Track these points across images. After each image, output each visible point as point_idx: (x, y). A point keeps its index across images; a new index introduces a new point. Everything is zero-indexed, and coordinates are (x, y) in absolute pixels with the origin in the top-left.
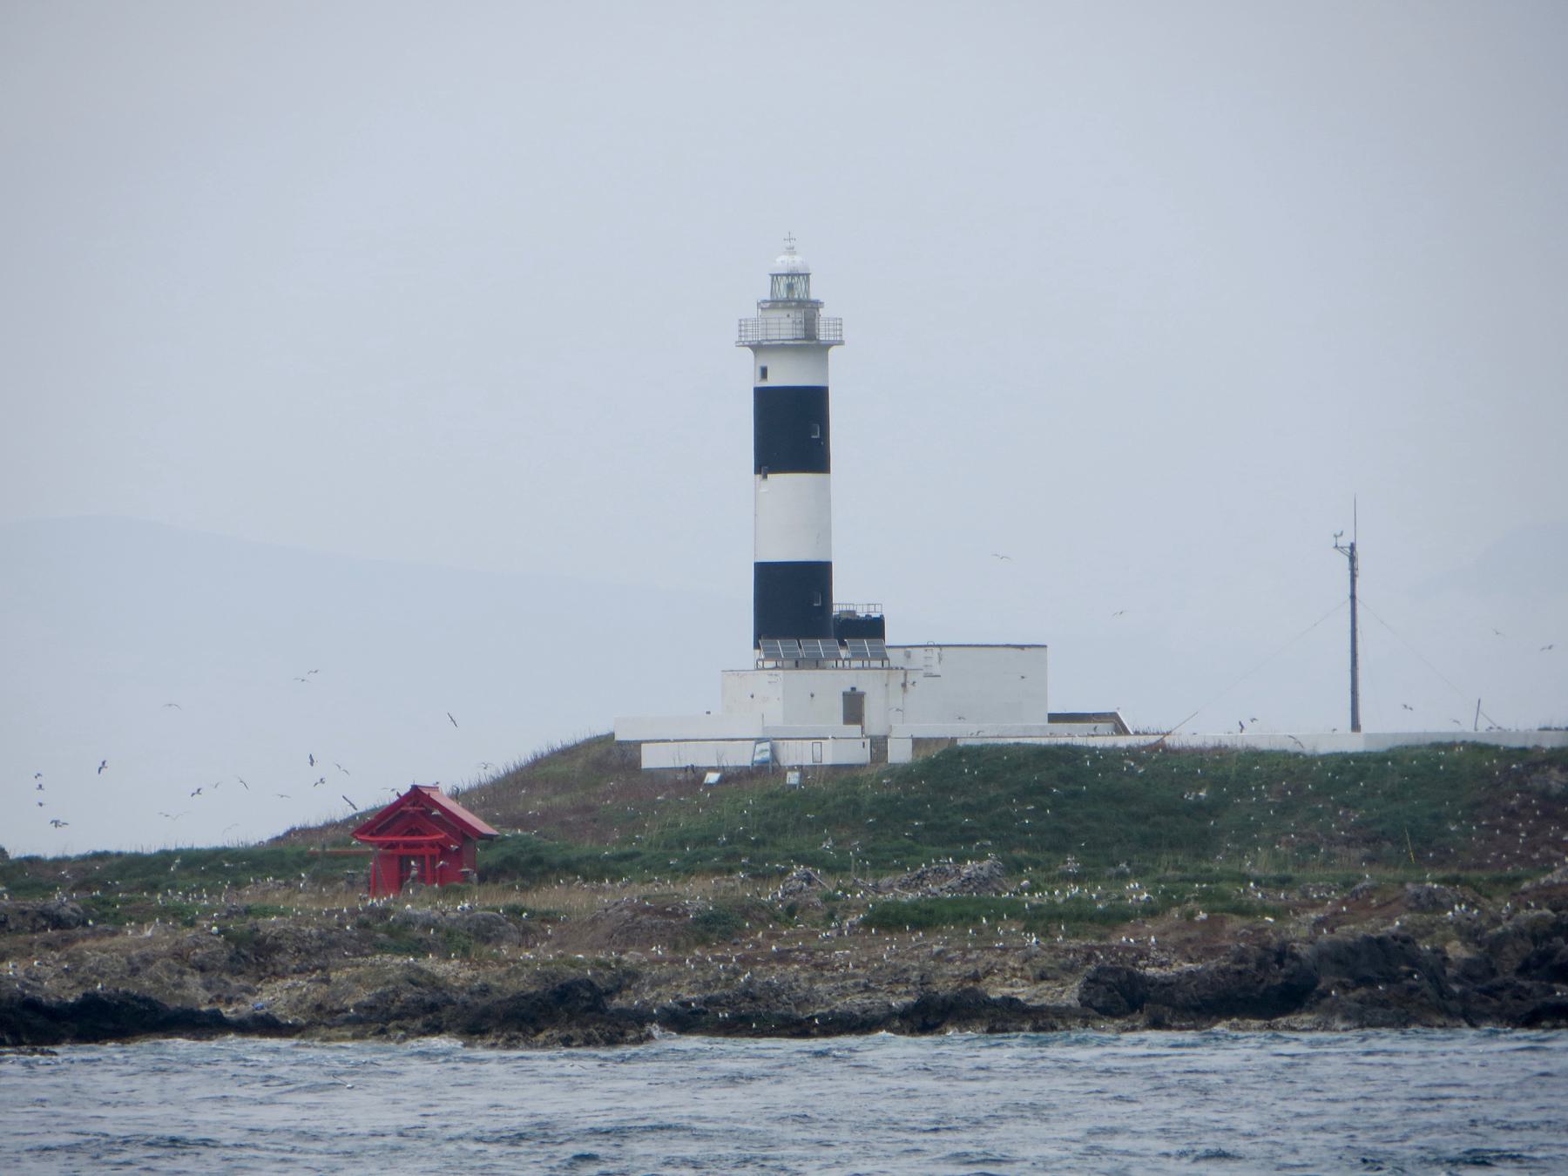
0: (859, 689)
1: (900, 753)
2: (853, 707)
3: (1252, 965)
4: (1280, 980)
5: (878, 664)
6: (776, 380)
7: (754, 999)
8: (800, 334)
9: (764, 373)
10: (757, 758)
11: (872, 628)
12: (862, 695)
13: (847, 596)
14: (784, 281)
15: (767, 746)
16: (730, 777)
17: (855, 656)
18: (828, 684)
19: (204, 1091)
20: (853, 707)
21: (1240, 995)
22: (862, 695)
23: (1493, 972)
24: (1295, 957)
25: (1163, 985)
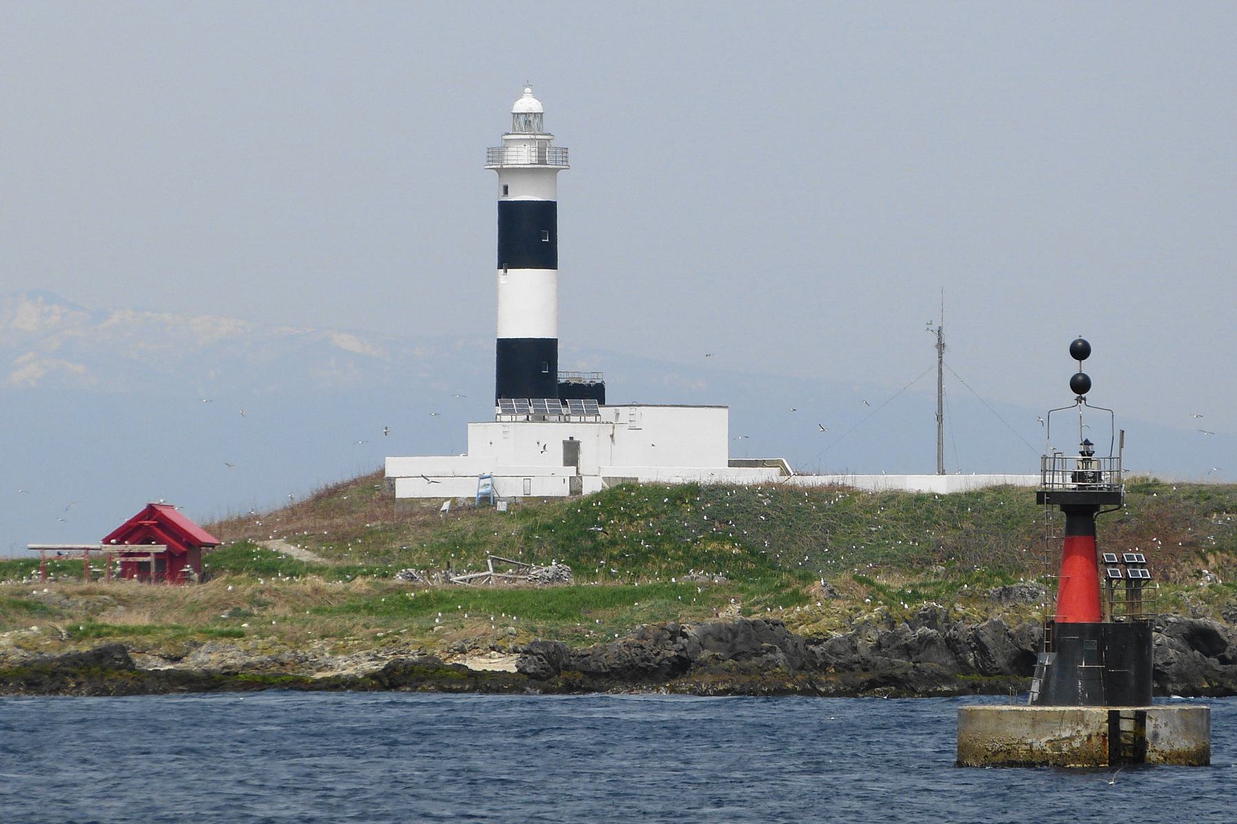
0: (576, 439)
1: (591, 486)
2: (572, 452)
3: (651, 641)
4: (673, 653)
5: (592, 419)
6: (514, 197)
7: (282, 664)
8: (534, 160)
9: (506, 192)
10: (482, 490)
11: (594, 393)
12: (578, 443)
13: (569, 368)
14: (522, 118)
15: (488, 481)
16: (458, 508)
17: (575, 413)
18: (555, 432)
19: (133, 742)
20: (572, 452)
21: (641, 665)
22: (578, 443)
23: (855, 650)
24: (685, 635)
25: (583, 656)
